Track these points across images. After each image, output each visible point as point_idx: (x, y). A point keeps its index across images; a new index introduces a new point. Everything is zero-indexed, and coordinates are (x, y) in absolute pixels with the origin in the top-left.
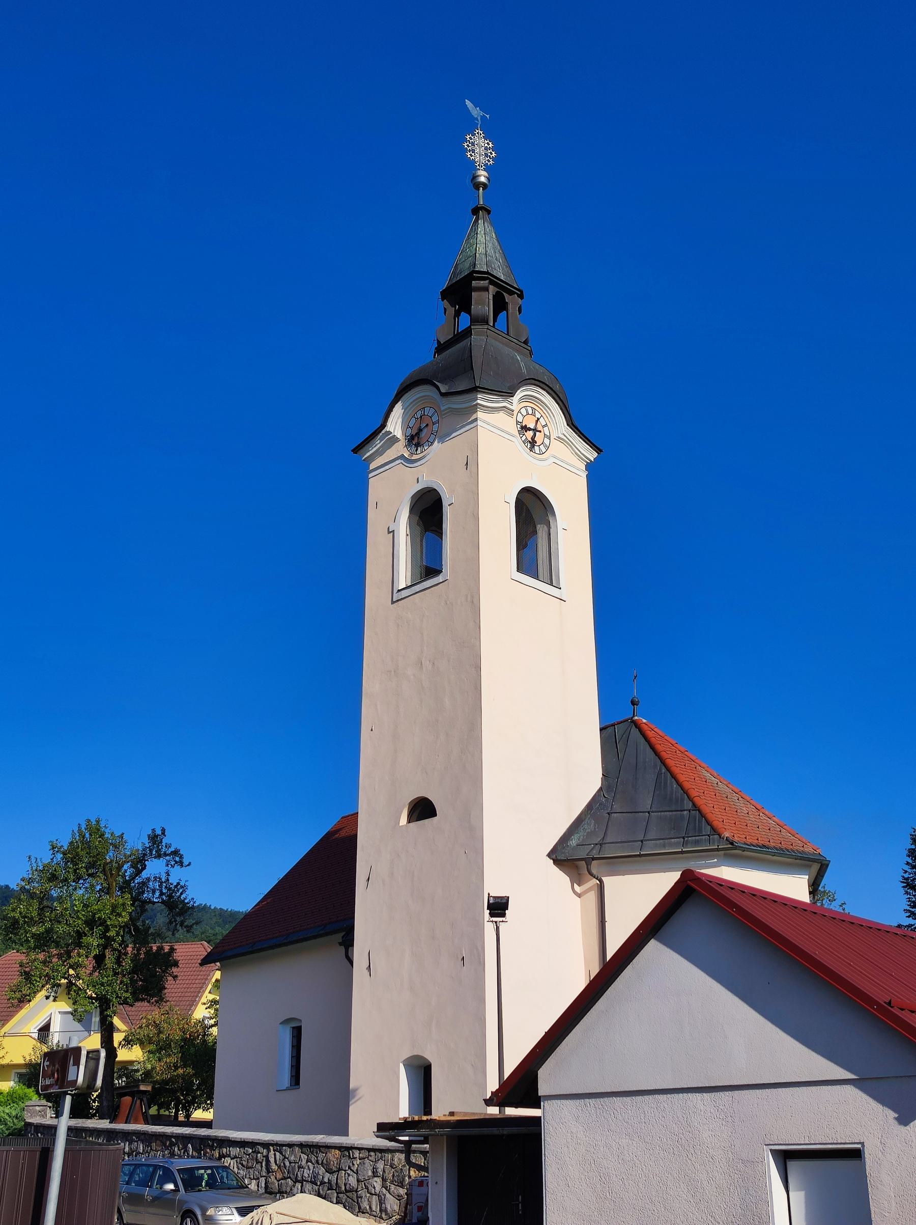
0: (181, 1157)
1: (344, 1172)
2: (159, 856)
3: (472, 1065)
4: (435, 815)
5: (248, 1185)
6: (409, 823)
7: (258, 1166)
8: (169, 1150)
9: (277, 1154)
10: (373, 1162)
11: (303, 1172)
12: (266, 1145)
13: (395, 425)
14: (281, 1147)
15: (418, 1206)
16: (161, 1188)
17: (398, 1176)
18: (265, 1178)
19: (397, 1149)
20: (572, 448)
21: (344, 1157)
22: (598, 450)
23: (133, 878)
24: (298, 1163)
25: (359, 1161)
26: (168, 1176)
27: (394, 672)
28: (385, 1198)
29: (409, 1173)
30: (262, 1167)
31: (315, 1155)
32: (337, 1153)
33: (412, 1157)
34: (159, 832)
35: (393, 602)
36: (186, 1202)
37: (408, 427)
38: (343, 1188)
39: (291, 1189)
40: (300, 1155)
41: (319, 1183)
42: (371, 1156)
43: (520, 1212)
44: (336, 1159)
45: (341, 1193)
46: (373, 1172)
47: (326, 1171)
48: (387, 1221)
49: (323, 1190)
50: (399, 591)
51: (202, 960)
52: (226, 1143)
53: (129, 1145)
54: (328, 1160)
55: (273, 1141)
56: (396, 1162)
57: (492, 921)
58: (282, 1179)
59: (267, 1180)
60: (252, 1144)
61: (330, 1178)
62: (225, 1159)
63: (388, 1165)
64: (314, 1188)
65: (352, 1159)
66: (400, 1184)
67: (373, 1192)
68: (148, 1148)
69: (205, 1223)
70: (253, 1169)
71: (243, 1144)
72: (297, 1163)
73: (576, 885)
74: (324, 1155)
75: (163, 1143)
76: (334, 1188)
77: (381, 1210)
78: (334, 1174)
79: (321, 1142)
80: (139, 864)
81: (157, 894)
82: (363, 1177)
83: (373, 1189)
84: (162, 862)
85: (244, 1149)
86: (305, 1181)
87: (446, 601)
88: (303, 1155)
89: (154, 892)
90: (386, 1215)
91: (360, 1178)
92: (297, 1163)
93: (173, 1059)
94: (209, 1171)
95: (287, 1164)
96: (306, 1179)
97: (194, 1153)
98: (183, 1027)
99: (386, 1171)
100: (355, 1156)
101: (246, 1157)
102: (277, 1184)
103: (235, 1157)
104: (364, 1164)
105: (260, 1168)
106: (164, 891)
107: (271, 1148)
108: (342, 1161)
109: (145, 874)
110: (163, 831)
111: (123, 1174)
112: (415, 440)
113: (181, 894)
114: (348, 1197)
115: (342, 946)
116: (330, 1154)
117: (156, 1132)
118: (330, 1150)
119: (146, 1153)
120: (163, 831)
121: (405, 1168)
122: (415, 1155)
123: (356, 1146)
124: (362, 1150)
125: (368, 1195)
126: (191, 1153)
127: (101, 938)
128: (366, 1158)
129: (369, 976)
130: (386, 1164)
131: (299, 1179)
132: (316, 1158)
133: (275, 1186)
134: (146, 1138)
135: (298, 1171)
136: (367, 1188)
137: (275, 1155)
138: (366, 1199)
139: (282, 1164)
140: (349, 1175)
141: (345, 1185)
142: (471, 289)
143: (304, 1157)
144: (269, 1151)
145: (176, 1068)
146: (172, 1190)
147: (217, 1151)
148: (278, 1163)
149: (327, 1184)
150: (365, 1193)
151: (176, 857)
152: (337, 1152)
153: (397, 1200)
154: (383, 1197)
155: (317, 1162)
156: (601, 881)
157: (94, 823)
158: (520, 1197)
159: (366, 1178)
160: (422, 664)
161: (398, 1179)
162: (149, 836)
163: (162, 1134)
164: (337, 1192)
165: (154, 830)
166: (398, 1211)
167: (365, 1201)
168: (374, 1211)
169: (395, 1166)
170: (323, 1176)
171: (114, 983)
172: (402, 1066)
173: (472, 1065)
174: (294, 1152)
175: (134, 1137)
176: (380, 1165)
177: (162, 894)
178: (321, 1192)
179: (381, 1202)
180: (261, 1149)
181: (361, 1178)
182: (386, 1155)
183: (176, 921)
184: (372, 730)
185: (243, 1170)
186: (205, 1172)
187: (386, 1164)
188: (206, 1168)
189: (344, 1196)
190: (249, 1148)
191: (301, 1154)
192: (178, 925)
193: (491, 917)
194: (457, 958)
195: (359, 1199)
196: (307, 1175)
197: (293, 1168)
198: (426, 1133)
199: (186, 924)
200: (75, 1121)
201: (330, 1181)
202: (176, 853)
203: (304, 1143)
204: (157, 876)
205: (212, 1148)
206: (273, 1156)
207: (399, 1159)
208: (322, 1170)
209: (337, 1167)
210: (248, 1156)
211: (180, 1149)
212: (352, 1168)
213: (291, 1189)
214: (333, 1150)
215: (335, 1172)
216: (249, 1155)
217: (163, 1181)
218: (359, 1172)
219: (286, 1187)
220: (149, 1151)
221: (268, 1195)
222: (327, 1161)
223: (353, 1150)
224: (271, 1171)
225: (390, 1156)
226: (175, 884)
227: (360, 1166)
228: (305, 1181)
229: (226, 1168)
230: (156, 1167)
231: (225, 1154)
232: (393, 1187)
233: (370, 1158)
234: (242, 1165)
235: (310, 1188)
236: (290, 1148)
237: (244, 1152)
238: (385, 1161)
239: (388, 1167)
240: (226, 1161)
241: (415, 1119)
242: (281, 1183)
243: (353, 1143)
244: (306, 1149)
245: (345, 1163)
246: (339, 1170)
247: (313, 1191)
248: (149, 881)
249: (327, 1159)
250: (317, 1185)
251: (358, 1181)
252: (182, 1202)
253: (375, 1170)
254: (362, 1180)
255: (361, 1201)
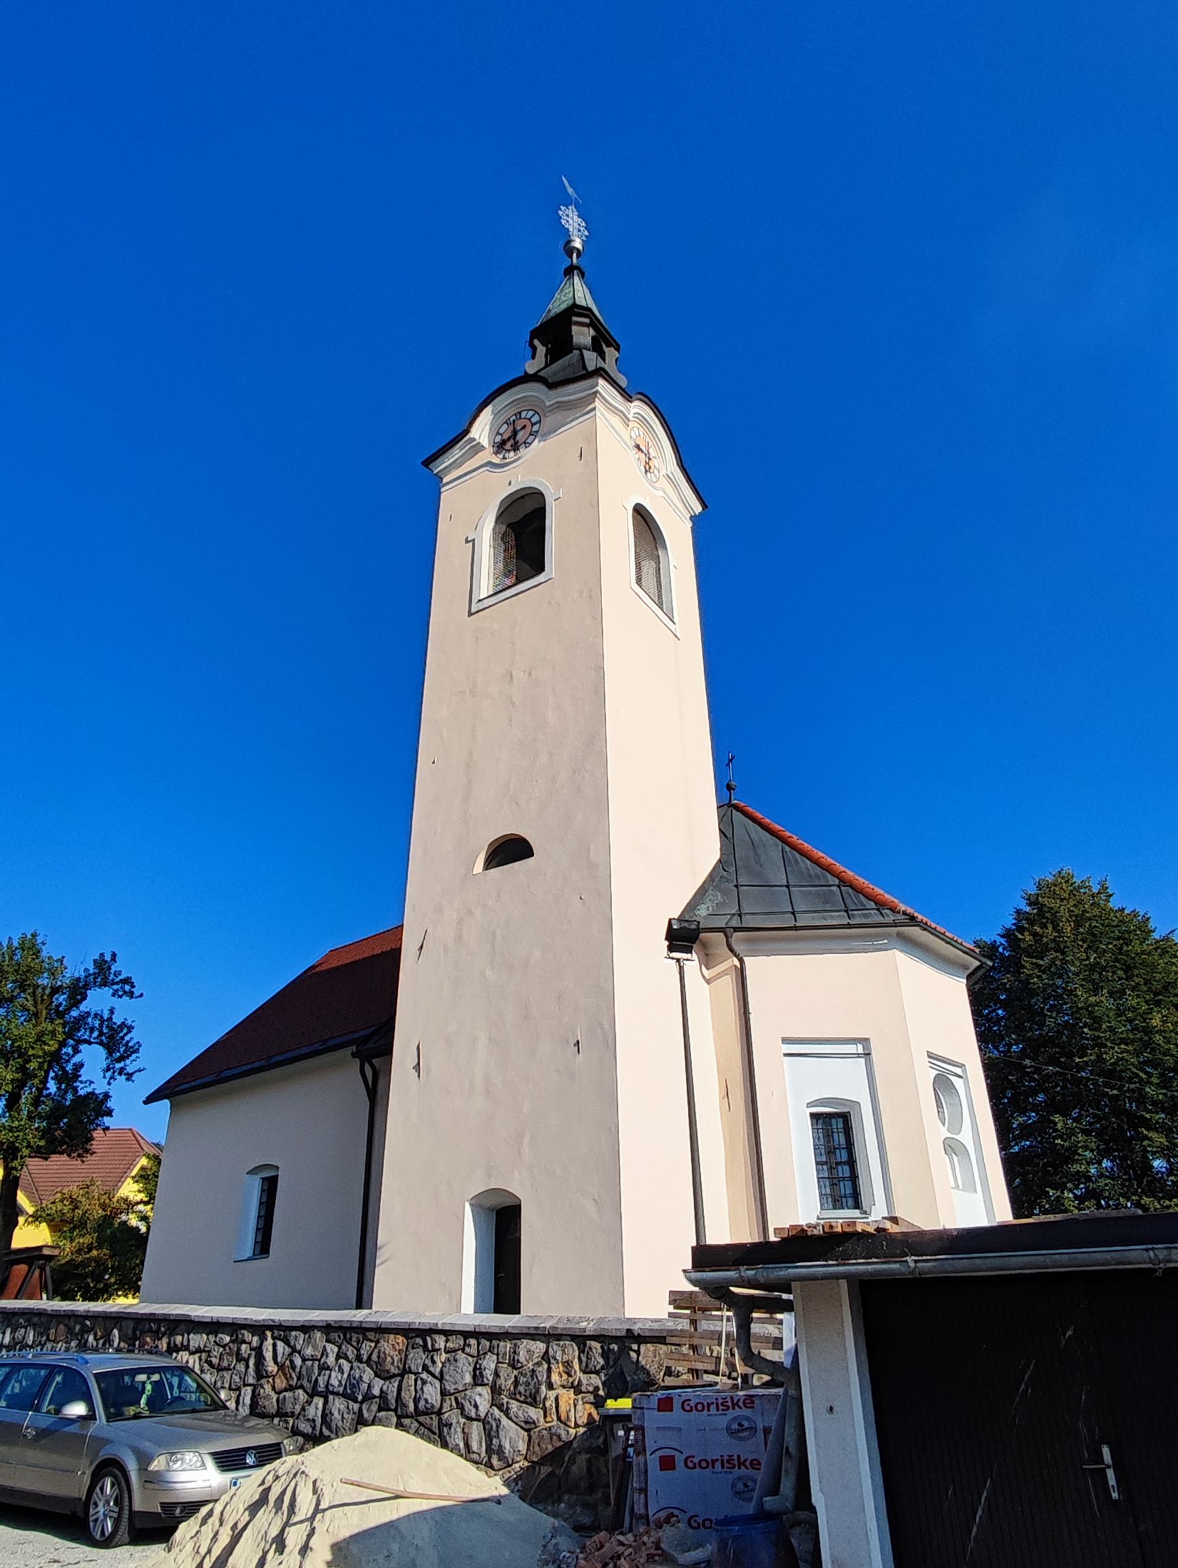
0: (98, 1351)
1: (413, 1377)
2: (104, 984)
3: (595, 1200)
4: (532, 855)
5: (226, 1401)
6: (486, 869)
7: (241, 1367)
8: (77, 1339)
9: (280, 1344)
10: (472, 1356)
11: (330, 1376)
12: (259, 1329)
13: (482, 430)
14: (287, 1332)
15: (660, 1457)
16: (58, 1411)
17: (527, 1384)
18: (252, 1388)
19: (526, 1331)
20: (679, 493)
21: (413, 1348)
22: (704, 505)
23: (68, 1009)
24: (319, 1360)
25: (444, 1356)
26: (75, 1387)
27: (470, 691)
28: (498, 1427)
29: (549, 1377)
30: (247, 1367)
31: (355, 1344)
32: (400, 1341)
33: (555, 1347)
34: (108, 958)
35: (470, 614)
36: (107, 1441)
37: (498, 433)
38: (411, 1408)
39: (303, 1409)
40: (324, 1346)
41: (360, 1398)
42: (469, 1346)
43: (1115, 1495)
44: (397, 1353)
45: (407, 1416)
46: (474, 1377)
47: (377, 1375)
48: (501, 1472)
49: (369, 1410)
50: (480, 601)
51: (148, 1098)
52: (183, 1326)
53: (11, 1333)
54: (382, 1355)
55: (272, 1320)
56: (522, 1356)
57: (673, 958)
58: (286, 1390)
59: (257, 1391)
60: (234, 1327)
61: (385, 1388)
62: (178, 1354)
63: (504, 1363)
64: (351, 1407)
65: (430, 1352)
66: (529, 1400)
67: (473, 1415)
68: (42, 1337)
69: (145, 1488)
70: (230, 1372)
71: (213, 1327)
72: (316, 1360)
73: (703, 968)
74: (373, 1345)
75: (69, 1329)
76: (393, 1408)
77: (489, 1450)
78: (392, 1381)
79: (366, 1322)
80: (78, 991)
81: (96, 1034)
82: (453, 1387)
83: (474, 1410)
84: (107, 991)
85: (216, 1337)
86: (333, 1393)
87: (550, 603)
88: (329, 1347)
89: (92, 1030)
90: (499, 1460)
91: (448, 1387)
92: (316, 1360)
93: (86, 1240)
94: (156, 1377)
95: (298, 1361)
96: (335, 1390)
97: (122, 1345)
98: (104, 1202)
99: (501, 1374)
100: (437, 1346)
101: (217, 1352)
102: (274, 1400)
103: (199, 1350)
104: (456, 1361)
105: (243, 1370)
106: (105, 1031)
107: (269, 1334)
108: (410, 1357)
109: (84, 1007)
110: (114, 955)
111: (1147, 956)
112: (509, 443)
113: (126, 1034)
114: (421, 1424)
115: (356, 1059)
116: (386, 1344)
117: (60, 1311)
118: (386, 1335)
119: (37, 1346)
120: (114, 955)
121: (540, 1369)
122: (562, 1343)
123: (440, 1327)
124: (451, 1335)
125: (462, 1421)
126: (116, 1344)
127: (17, 1071)
128: (459, 1350)
129: (417, 1078)
130: (500, 1360)
131: (320, 1389)
132: (355, 1352)
133: (272, 1403)
134: (42, 1321)
135: (319, 1375)
136: (461, 1407)
137: (274, 1345)
138: (459, 1430)
139: (288, 1363)
140: (424, 1382)
141: (416, 1401)
142: (570, 323)
143: (332, 1349)
144: (263, 1339)
145: (90, 1250)
146: (80, 1417)
147: (165, 1341)
148: (279, 1359)
149: (377, 1400)
150: (457, 1417)
151: (126, 988)
152: (400, 1339)
153: (522, 1432)
154: (494, 1425)
155: (359, 1359)
156: (741, 961)
157: (29, 937)
158: (1106, 1451)
159: (460, 1389)
160: (512, 677)
161: (526, 1390)
162: (95, 961)
163: (70, 1313)
164: (396, 1415)
165: (102, 955)
166: (524, 1452)
167: (456, 1432)
168: (474, 1452)
169: (519, 1365)
170: (369, 1385)
171: (26, 1129)
172: (468, 1207)
173: (595, 1200)
174: (313, 1341)
175: (21, 1320)
176: (489, 1363)
177: (101, 1034)
178: (366, 1414)
179: (491, 1431)
180: (247, 1336)
181: (450, 1387)
182: (502, 1344)
183: (113, 1068)
184: (434, 762)
185: (211, 1374)
186: (149, 1378)
187: (500, 1360)
188: (150, 1371)
189: (412, 1423)
190: (224, 1334)
191: (327, 1344)
192: (116, 1074)
193: (671, 952)
194: (567, 1042)
195: (445, 1430)
196: (336, 1383)
197: (310, 1370)
198: (869, 1267)
199: (126, 1072)
200: (45, 1360)
201: (383, 1394)
202: (127, 981)
203: (333, 1324)
204: (99, 1012)
205: (157, 1336)
206: (270, 1348)
207: (529, 1351)
208: (368, 1374)
209: (398, 1367)
210: (221, 1349)
211: (98, 1337)
212: (431, 1369)
213: (303, 1409)
214: (392, 1336)
215: (394, 1376)
216: (224, 1346)
217: (61, 1401)
218: (447, 1377)
219: (294, 1404)
220: (43, 1342)
221: (259, 1421)
222: (379, 1357)
223: (434, 1336)
224: (264, 1374)
225: (509, 1345)
226: (119, 1023)
227: (448, 1365)
228: (333, 1393)
229: (185, 1370)
230: (53, 1369)
231: (180, 1346)
232: (514, 1405)
233: (467, 1350)
234: (210, 1364)
235: (342, 1407)
236: (305, 1334)
237: (215, 1342)
238: (498, 1355)
239: (505, 1365)
240: (179, 1357)
241: (835, 1230)
242: (285, 1397)
243: (435, 1322)
244: (337, 1334)
245: (417, 1359)
246: (405, 1371)
247: (349, 1413)
248: (88, 1017)
249: (379, 1352)
250: (355, 1401)
251: (444, 1393)
252: (101, 1441)
253: (478, 1372)
254: (452, 1391)
255: (448, 1433)
